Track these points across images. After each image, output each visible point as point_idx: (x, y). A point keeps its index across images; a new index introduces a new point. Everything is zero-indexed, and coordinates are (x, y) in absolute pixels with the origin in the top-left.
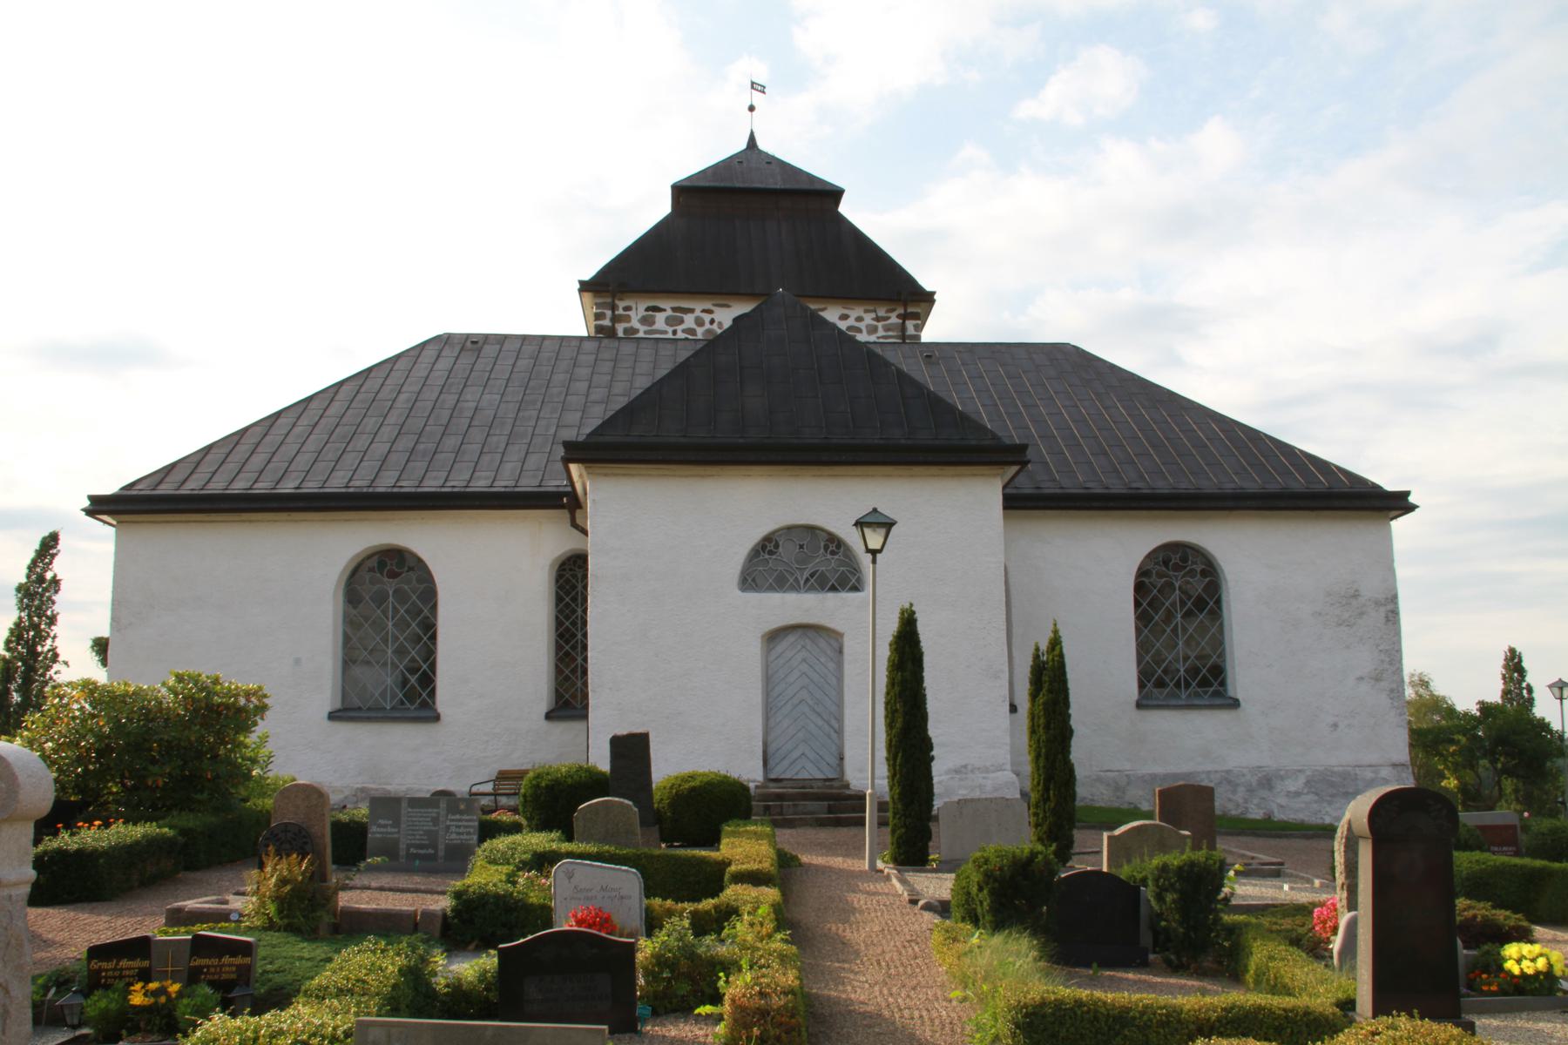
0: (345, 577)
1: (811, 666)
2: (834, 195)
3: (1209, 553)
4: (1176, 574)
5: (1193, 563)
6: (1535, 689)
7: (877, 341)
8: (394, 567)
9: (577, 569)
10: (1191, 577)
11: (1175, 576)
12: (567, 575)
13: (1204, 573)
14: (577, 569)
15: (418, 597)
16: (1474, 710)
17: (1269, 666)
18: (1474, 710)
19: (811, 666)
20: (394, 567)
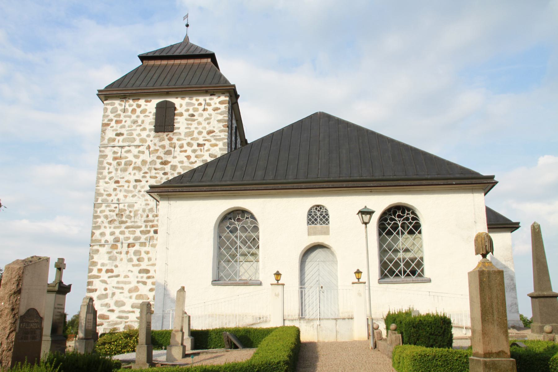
0: (225, 214)
1: (201, 361)
2: (155, 108)
3: (393, 204)
4: (399, 219)
5: (408, 214)
6: (352, 320)
7: (192, 122)
8: (400, 213)
9: (397, 219)
10: (407, 221)
11: (398, 220)
12: (313, 214)
13: (413, 219)
14: (397, 219)
15: (226, 243)
16: (65, 263)
17: (156, 260)
18: (65, 263)
19: (201, 361)
20: (400, 213)
